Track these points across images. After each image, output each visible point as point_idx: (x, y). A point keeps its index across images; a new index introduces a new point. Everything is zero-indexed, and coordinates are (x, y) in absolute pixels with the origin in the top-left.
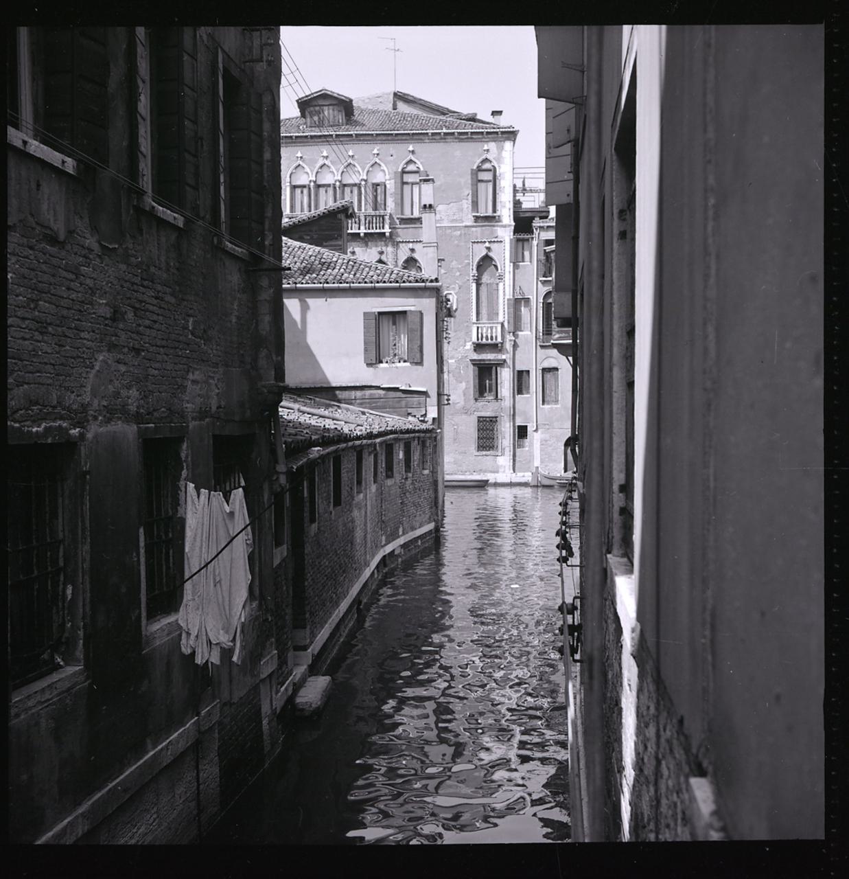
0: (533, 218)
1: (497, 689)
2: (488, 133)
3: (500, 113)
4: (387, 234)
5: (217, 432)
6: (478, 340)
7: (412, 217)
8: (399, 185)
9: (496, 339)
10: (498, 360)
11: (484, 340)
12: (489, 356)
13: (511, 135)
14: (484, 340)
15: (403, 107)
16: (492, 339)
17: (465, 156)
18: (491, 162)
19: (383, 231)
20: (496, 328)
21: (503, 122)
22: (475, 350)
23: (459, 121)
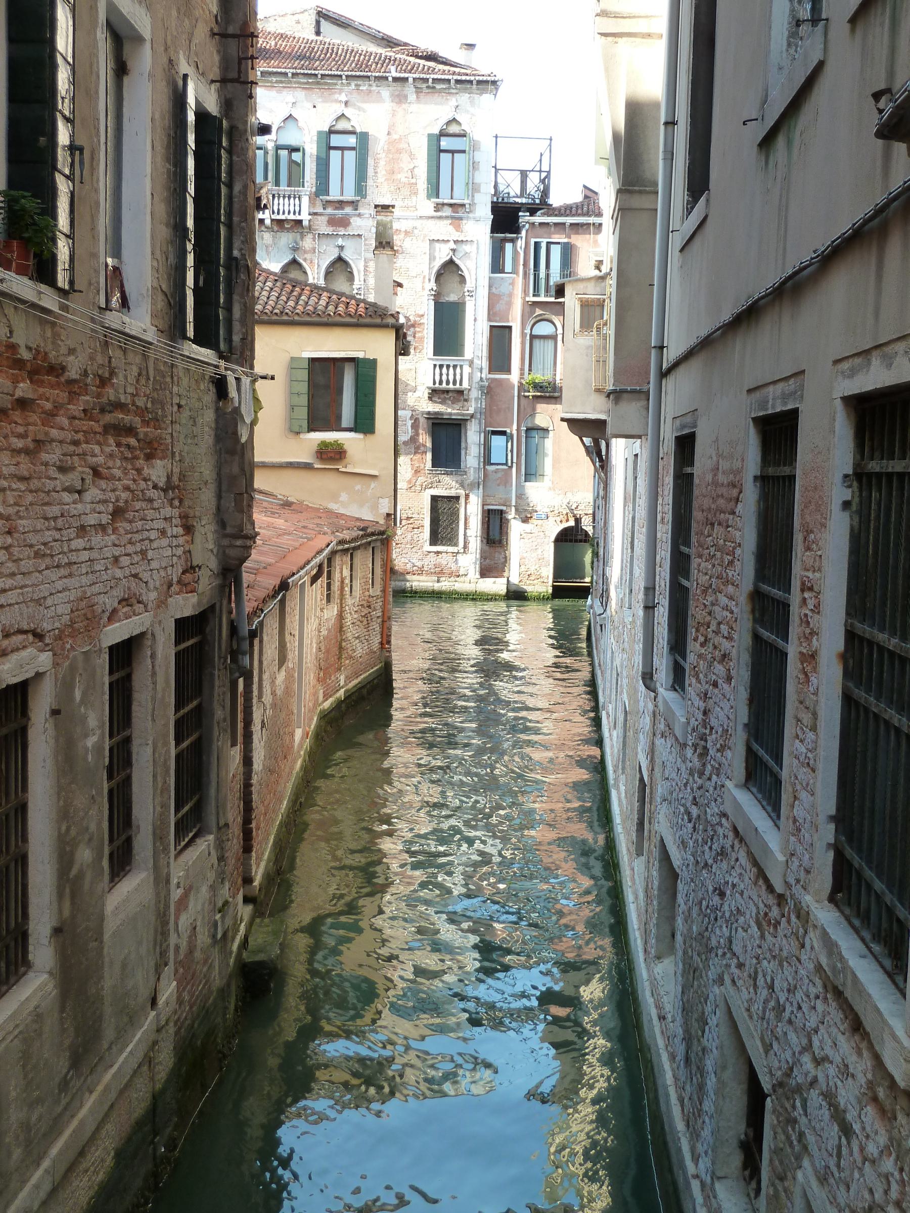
0: (519, 209)
1: (415, 891)
2: (457, 81)
3: (471, 46)
4: (306, 223)
5: (305, 424)
6: (434, 383)
7: (341, 198)
8: (435, 152)
9: (461, 384)
10: (463, 415)
11: (444, 385)
12: (448, 410)
13: (488, 84)
14: (444, 385)
15: (332, 35)
16: (455, 383)
17: (427, 115)
18: (349, 119)
19: (299, 218)
20: (461, 367)
21: (481, 64)
22: (430, 399)
23: (412, 59)
